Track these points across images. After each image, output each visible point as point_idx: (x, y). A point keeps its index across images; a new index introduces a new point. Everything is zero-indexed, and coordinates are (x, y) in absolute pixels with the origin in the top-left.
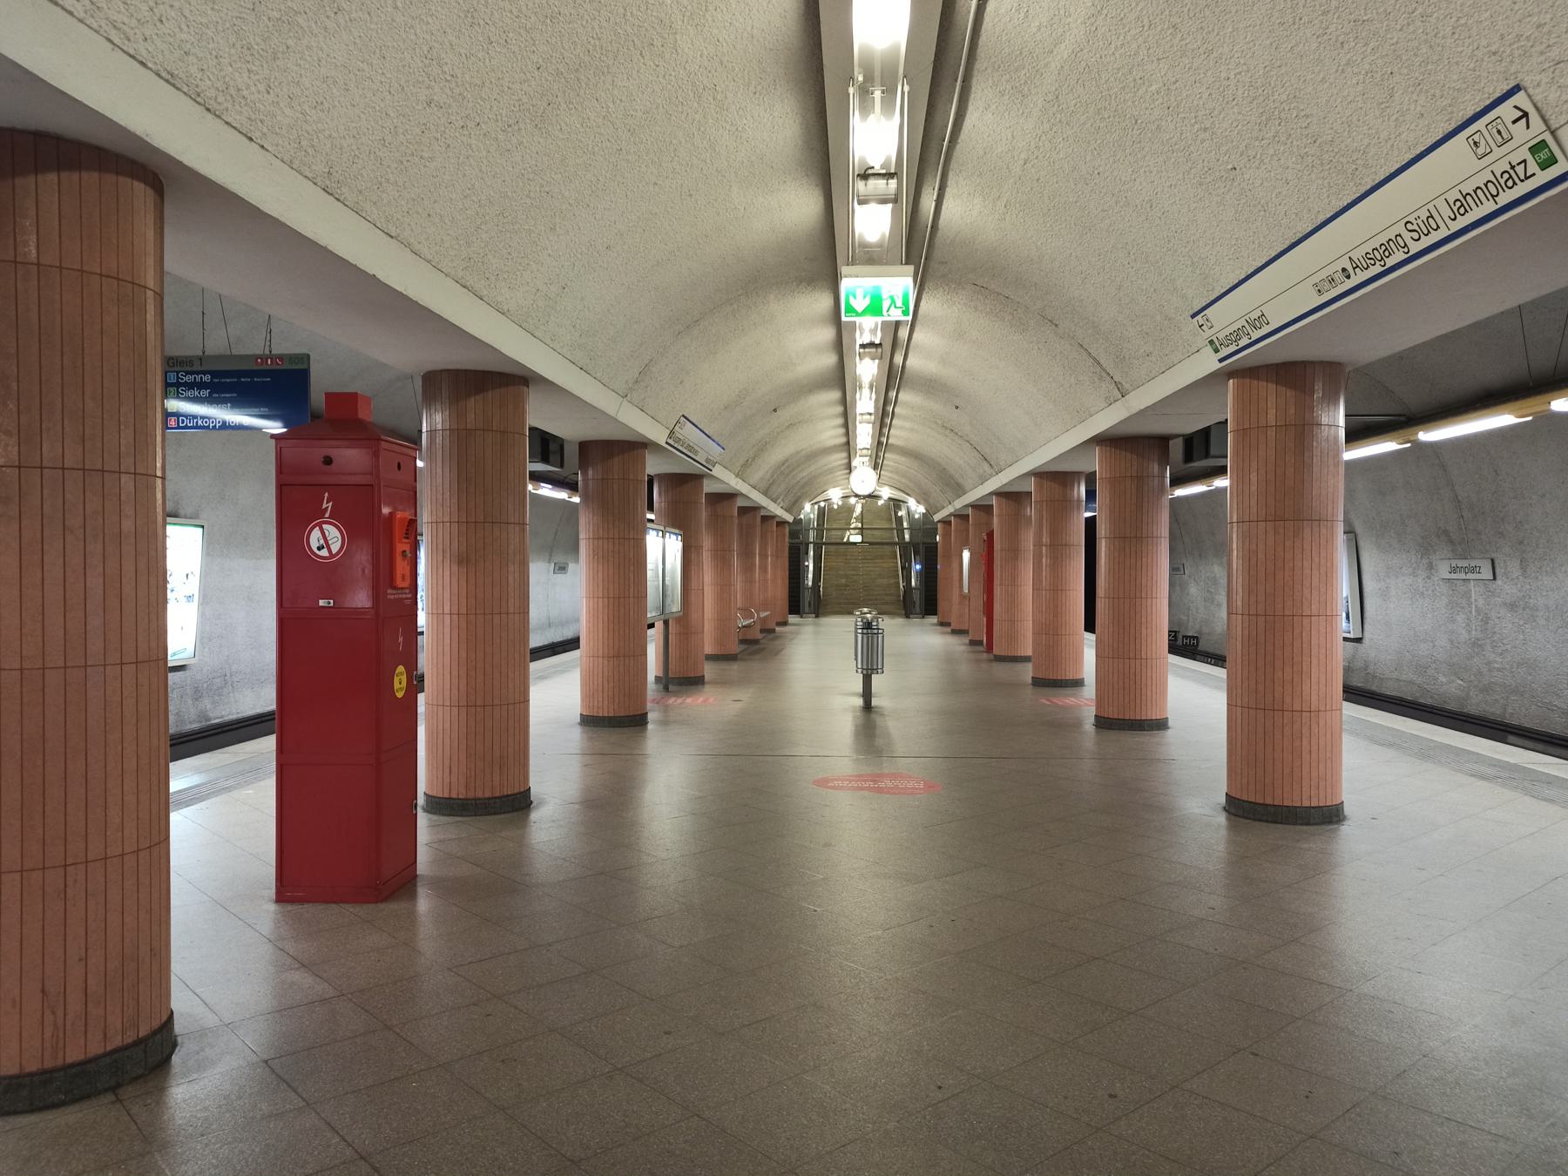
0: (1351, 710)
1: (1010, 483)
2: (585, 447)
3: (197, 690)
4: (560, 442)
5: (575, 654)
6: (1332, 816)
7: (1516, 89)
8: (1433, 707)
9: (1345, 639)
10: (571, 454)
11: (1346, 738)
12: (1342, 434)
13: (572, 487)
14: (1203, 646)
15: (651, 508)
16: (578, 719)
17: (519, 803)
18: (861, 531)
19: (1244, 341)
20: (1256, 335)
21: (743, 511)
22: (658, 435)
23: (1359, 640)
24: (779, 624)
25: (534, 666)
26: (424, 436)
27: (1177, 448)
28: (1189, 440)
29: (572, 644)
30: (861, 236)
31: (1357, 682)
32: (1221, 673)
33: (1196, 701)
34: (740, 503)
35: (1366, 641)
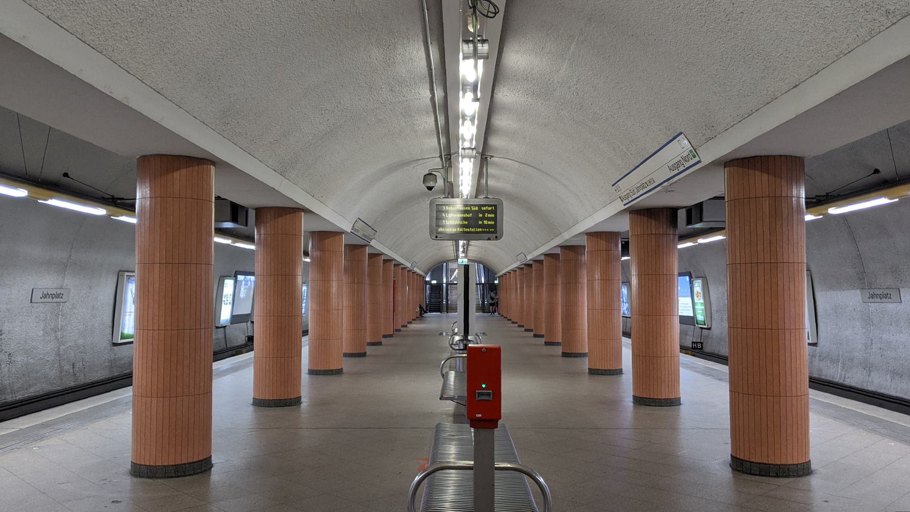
0: (815, 395)
1: (668, 185)
2: (259, 211)
3: (490, 288)
4: (246, 210)
5: (127, 394)
6: (804, 470)
7: (681, 133)
8: (850, 387)
9: (809, 344)
10: (252, 214)
11: (811, 415)
12: (803, 201)
13: (250, 239)
14: (707, 349)
15: (306, 254)
16: (252, 401)
17: (204, 466)
18: (466, 257)
19: (682, 168)
20: (687, 165)
21: (385, 261)
22: (346, 226)
23: (815, 344)
24: (403, 326)
25: (216, 366)
26: (137, 201)
27: (682, 215)
28: (689, 210)
29: (122, 380)
30: (464, 77)
31: (815, 375)
32: (725, 369)
33: (704, 393)
34: (383, 257)
35: (821, 342)
